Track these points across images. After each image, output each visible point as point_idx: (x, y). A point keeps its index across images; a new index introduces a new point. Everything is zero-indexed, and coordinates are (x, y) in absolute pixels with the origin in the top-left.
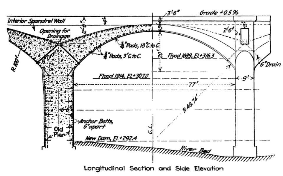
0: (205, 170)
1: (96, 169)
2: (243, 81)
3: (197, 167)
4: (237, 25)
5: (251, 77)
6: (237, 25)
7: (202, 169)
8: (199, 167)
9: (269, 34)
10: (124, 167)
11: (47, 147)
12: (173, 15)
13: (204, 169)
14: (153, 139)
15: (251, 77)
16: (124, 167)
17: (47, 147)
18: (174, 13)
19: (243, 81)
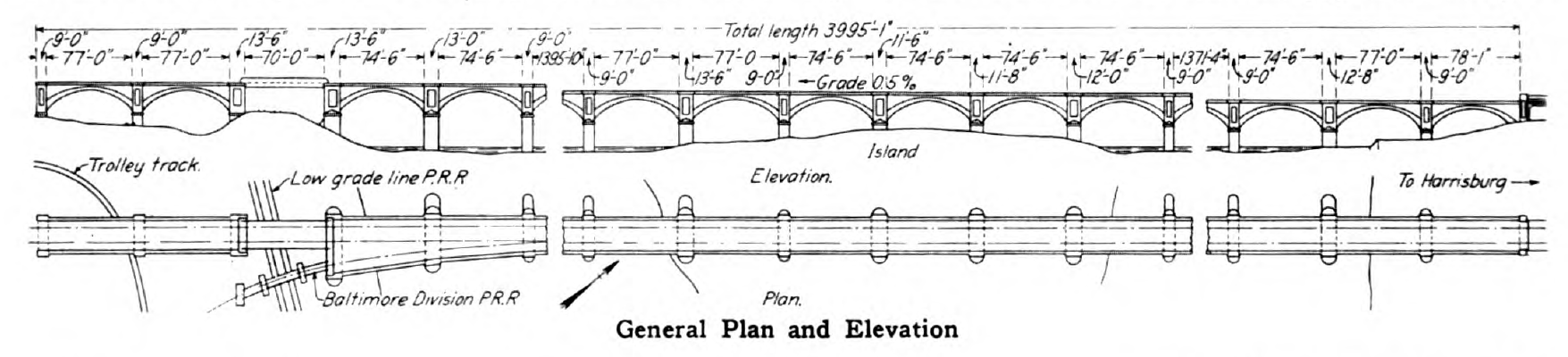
0: (891, 334)
1: (1480, 183)
2: (1498, 192)
3: (750, 336)
4: (438, 78)
5: (1102, 63)
6: (438, 78)
7: (881, 329)
8: (868, 322)
9: (1069, 137)
10: (1401, 185)
11: (35, 167)
12: (1154, 135)
13: (886, 330)
14: (1513, 182)
15: (1102, 63)
16: (1401, 185)
17: (35, 167)
18: (837, 56)
19: (1498, 192)
